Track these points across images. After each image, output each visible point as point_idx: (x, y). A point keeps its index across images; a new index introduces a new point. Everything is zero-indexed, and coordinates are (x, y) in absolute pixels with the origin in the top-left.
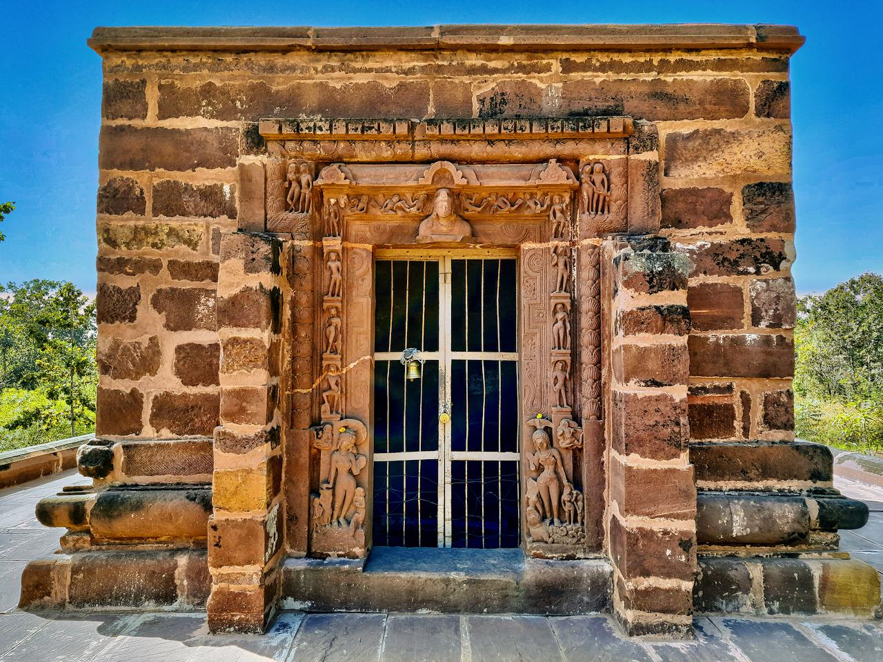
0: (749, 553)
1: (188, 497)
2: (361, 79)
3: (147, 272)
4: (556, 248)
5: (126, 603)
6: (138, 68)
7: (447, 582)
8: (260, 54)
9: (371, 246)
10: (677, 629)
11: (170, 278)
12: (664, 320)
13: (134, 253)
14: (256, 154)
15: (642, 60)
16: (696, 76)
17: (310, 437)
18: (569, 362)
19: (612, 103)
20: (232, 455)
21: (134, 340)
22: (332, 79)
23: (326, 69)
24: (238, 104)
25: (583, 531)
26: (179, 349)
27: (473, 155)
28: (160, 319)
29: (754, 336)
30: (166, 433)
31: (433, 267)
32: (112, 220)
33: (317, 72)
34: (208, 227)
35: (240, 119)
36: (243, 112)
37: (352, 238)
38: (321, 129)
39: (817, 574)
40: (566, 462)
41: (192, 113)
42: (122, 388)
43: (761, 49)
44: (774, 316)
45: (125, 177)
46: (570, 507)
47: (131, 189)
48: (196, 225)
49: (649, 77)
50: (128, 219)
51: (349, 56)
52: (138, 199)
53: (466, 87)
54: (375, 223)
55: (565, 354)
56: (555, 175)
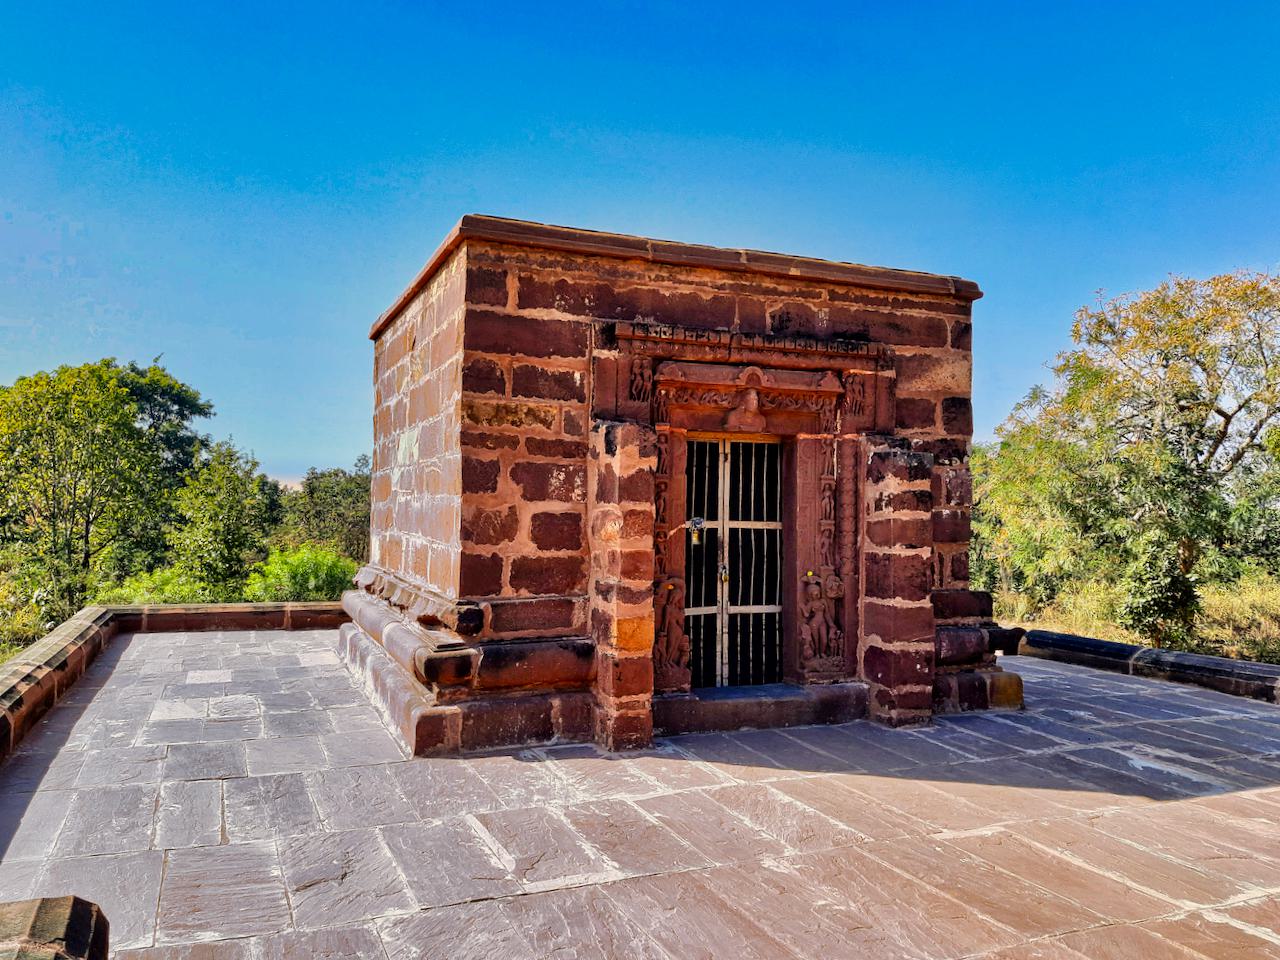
0: (945, 671)
1: (561, 647)
2: (686, 290)
3: (506, 447)
5: (512, 743)
6: (500, 259)
7: (760, 704)
8: (605, 259)
10: (923, 721)
11: (527, 453)
12: (918, 501)
13: (495, 429)
14: (610, 350)
15: (882, 296)
16: (915, 313)
18: (833, 530)
19: (861, 328)
20: (630, 605)
21: (495, 509)
22: (662, 287)
23: (659, 278)
24: (587, 301)
26: (535, 517)
27: (772, 363)
28: (518, 489)
29: (948, 512)
30: (524, 592)
31: (714, 447)
32: (475, 398)
33: (651, 280)
34: (561, 409)
35: (587, 315)
36: (591, 309)
38: (665, 333)
39: (988, 682)
41: (548, 306)
42: (484, 553)
43: (955, 297)
44: (960, 496)
45: (488, 358)
47: (493, 370)
48: (551, 406)
49: (886, 310)
50: (490, 398)
51: (676, 269)
52: (499, 380)
53: (762, 304)
54: (691, 412)
55: (830, 525)
56: (831, 384)
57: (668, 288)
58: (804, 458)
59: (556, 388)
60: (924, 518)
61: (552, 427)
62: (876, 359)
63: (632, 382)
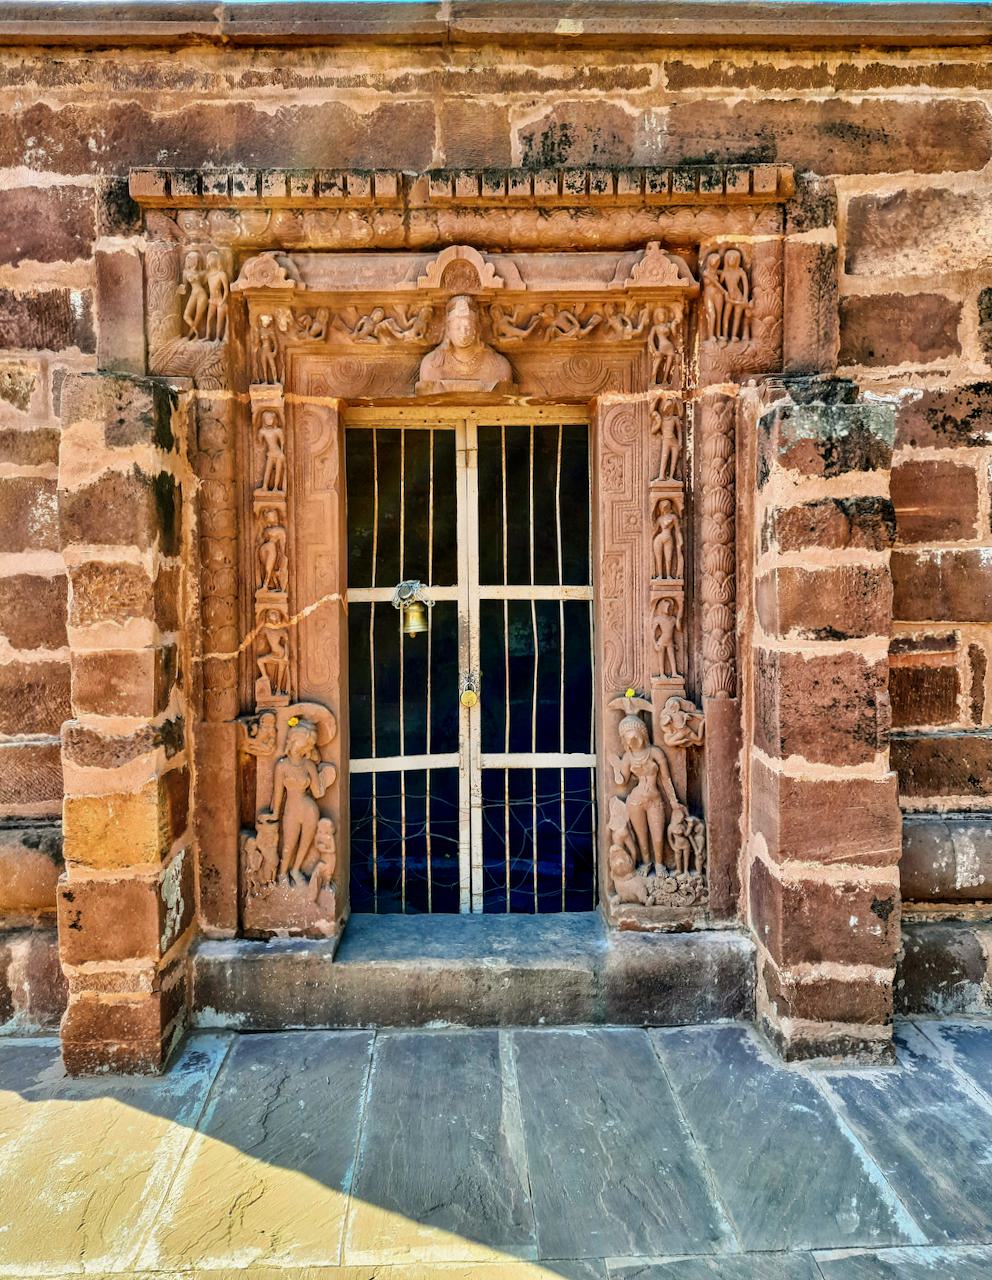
4: (659, 401)
7: (476, 975)
9: (335, 401)
10: (867, 1048)
12: (851, 524)
14: (126, 234)
15: (808, 65)
16: (901, 94)
17: (237, 736)
20: (96, 770)
23: (248, 80)
24: (92, 143)
25: (704, 884)
31: (447, 439)
33: (232, 85)
34: (45, 368)
35: (95, 172)
37: (302, 387)
40: (675, 769)
46: (682, 844)
51: (290, 55)
53: (500, 115)
54: (343, 360)
56: (660, 271)
57: (274, 98)
58: (614, 446)
59: (34, 325)
60: (867, 564)
61: (29, 406)
62: (781, 205)
63: (184, 299)
